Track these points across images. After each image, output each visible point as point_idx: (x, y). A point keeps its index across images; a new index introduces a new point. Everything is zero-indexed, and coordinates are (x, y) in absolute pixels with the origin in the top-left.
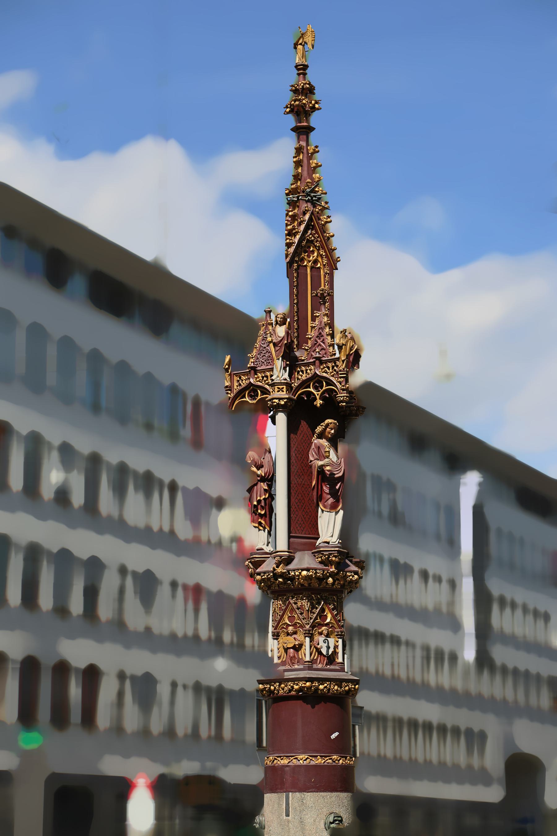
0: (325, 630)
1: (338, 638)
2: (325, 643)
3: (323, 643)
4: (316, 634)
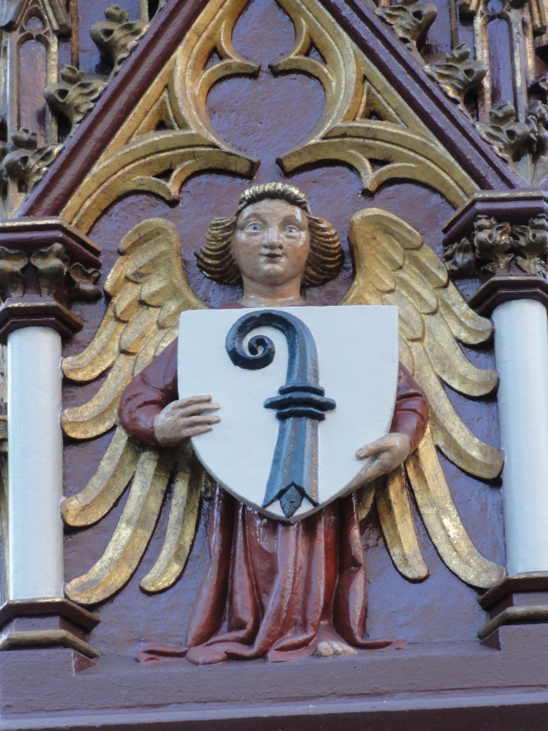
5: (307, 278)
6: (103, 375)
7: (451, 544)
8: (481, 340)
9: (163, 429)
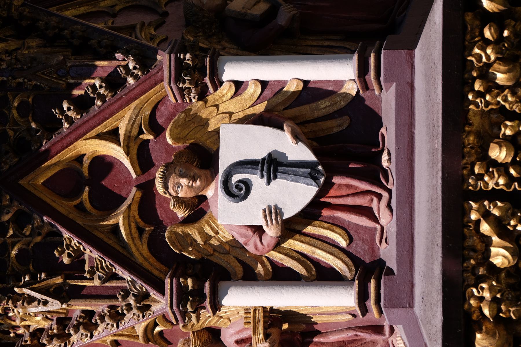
0: (171, 190)
1: (218, 83)
2: (247, 185)
3: (253, 192)
4: (202, 233)
5: (198, 166)
6: (239, 261)
7: (333, 105)
8: (234, 86)
9: (277, 233)
